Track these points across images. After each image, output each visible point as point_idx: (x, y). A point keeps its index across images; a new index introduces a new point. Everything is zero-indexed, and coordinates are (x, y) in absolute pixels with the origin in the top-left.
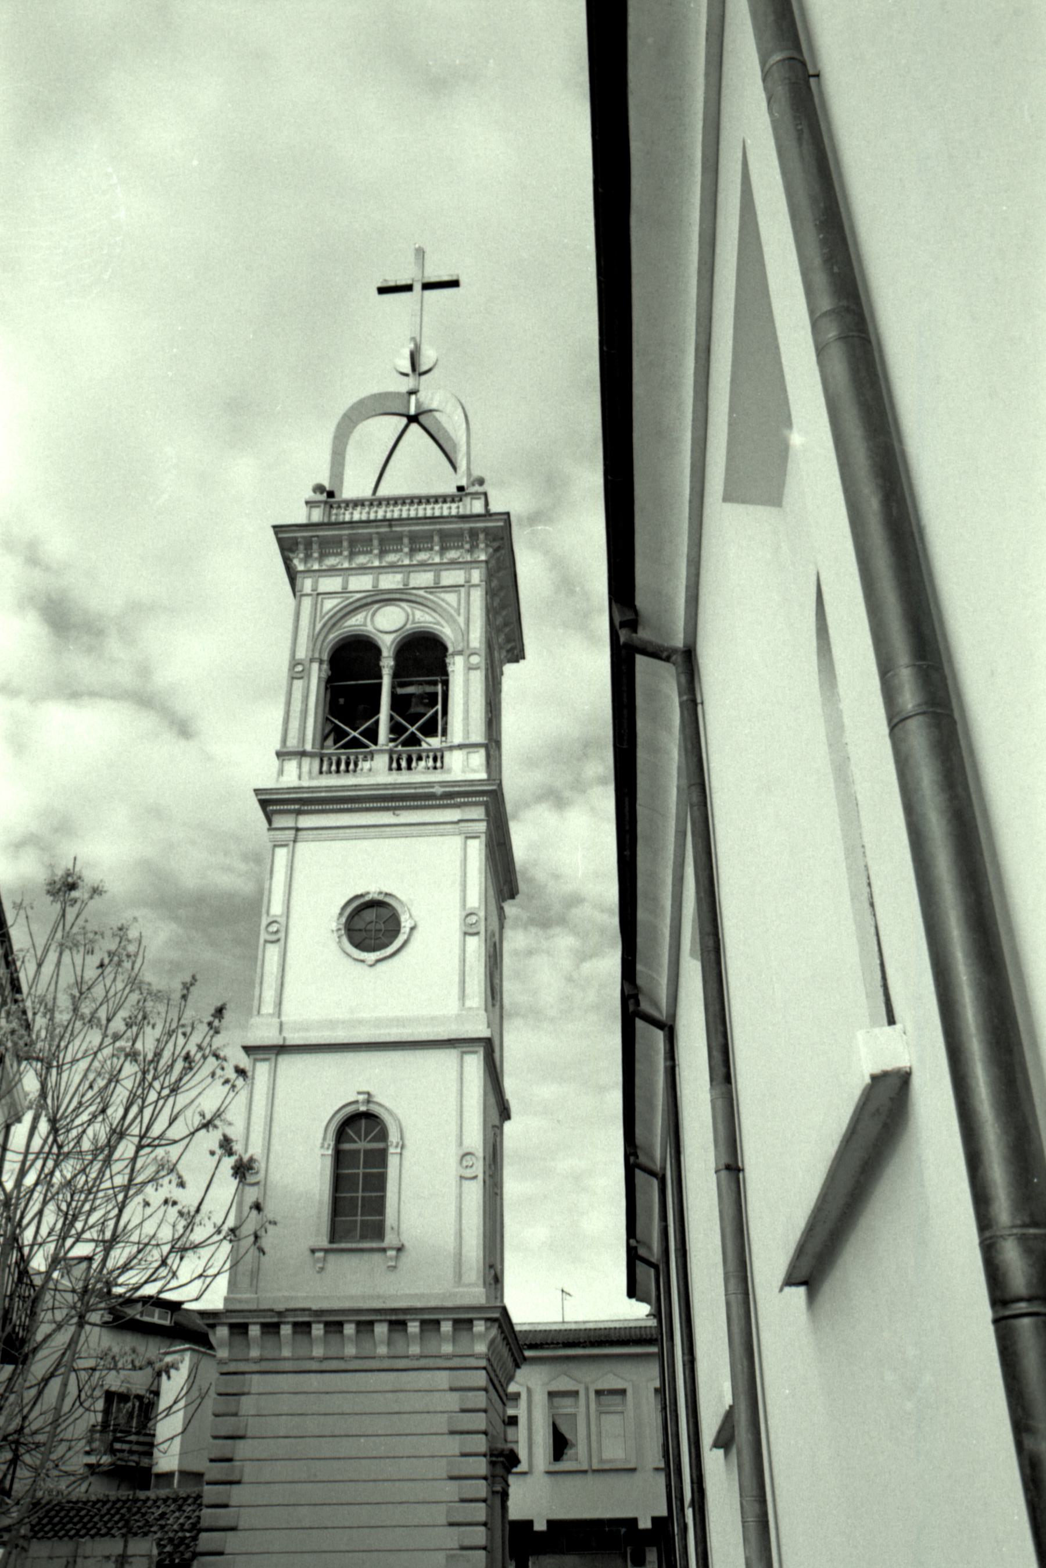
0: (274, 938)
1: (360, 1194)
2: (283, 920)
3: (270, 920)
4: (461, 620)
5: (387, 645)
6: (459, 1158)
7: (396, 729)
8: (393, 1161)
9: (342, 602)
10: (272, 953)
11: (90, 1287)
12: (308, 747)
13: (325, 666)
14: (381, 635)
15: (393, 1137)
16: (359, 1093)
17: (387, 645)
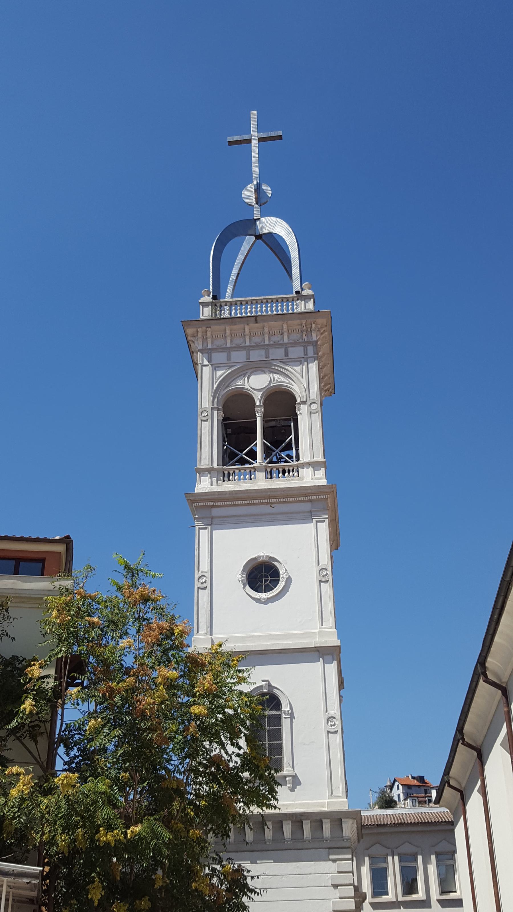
0: (204, 586)
1: (267, 743)
2: (208, 575)
3: (200, 575)
4: (304, 381)
5: (258, 398)
6: (326, 719)
7: (267, 452)
8: (285, 723)
9: (227, 371)
10: (204, 596)
11: (52, 787)
12: (215, 465)
13: (221, 412)
14: (256, 392)
15: (285, 707)
16: (263, 681)
17: (258, 398)
